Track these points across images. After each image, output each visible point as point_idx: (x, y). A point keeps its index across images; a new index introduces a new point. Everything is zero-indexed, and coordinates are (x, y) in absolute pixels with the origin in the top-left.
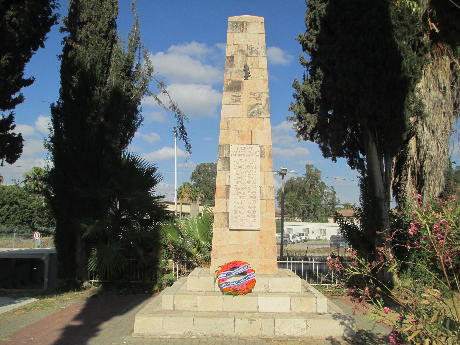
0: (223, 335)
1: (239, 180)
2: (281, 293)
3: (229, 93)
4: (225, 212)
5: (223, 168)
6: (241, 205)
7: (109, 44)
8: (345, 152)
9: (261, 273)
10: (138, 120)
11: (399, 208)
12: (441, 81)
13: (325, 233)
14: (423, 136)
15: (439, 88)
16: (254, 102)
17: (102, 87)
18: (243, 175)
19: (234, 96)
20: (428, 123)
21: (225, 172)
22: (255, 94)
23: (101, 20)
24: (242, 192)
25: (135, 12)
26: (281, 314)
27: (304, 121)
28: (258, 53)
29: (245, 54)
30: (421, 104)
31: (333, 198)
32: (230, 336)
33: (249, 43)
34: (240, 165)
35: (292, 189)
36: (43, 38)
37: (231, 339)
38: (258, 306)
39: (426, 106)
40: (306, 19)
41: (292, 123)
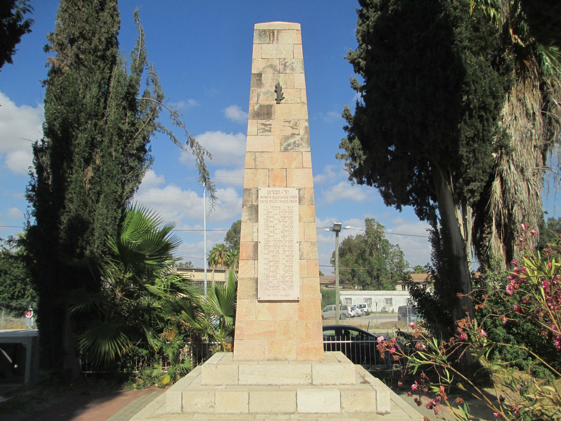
1: (271, 234)
2: (328, 385)
3: (256, 121)
6: (274, 267)
7: (109, 65)
8: (411, 199)
11: (481, 270)
12: (529, 106)
13: (391, 303)
14: (510, 176)
15: (527, 114)
16: (289, 131)
17: (98, 119)
19: (263, 124)
20: (515, 159)
21: (251, 223)
22: (290, 121)
23: (97, 36)
24: (275, 250)
25: (138, 24)
26: (329, 415)
27: (358, 160)
28: (293, 69)
29: (277, 71)
30: (505, 135)
31: (400, 260)
34: (271, 215)
35: (350, 251)
36: (11, 51)
38: (297, 405)
39: (511, 137)
40: (358, 32)
41: (343, 161)
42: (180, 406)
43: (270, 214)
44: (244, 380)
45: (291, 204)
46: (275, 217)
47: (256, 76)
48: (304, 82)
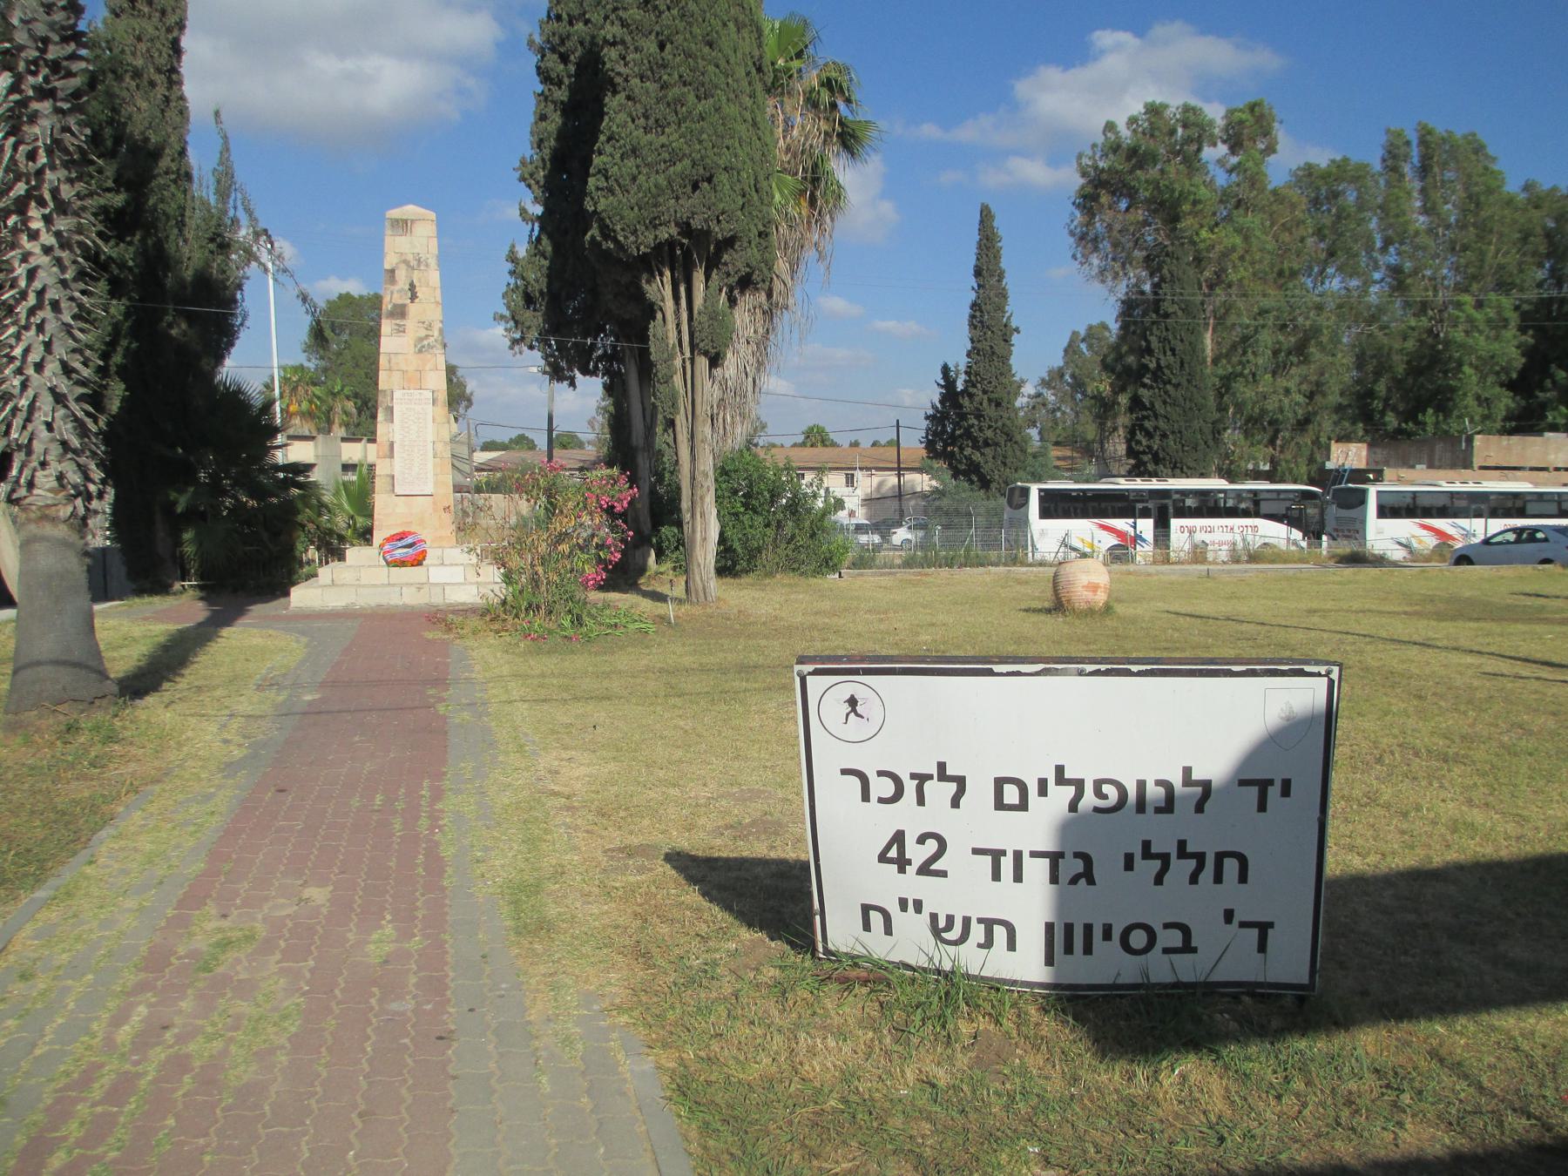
16: (423, 333)
28: (427, 265)
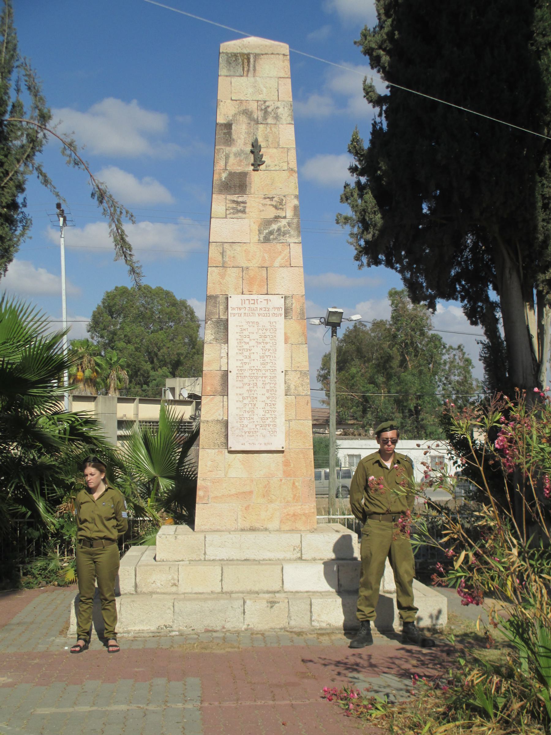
0: (224, 628)
1: (245, 360)
3: (223, 196)
4: (220, 418)
5: (216, 339)
9: (287, 528)
10: (19, 224)
16: (271, 213)
18: (252, 352)
19: (233, 201)
21: (218, 345)
22: (273, 197)
24: (251, 382)
28: (277, 117)
29: (254, 120)
32: (236, 629)
33: (260, 97)
34: (246, 333)
37: (239, 633)
38: (283, 582)
41: (348, 228)
42: (134, 584)
43: (244, 332)
44: (212, 553)
45: (273, 319)
46: (252, 336)
47: (223, 127)
48: (293, 138)
